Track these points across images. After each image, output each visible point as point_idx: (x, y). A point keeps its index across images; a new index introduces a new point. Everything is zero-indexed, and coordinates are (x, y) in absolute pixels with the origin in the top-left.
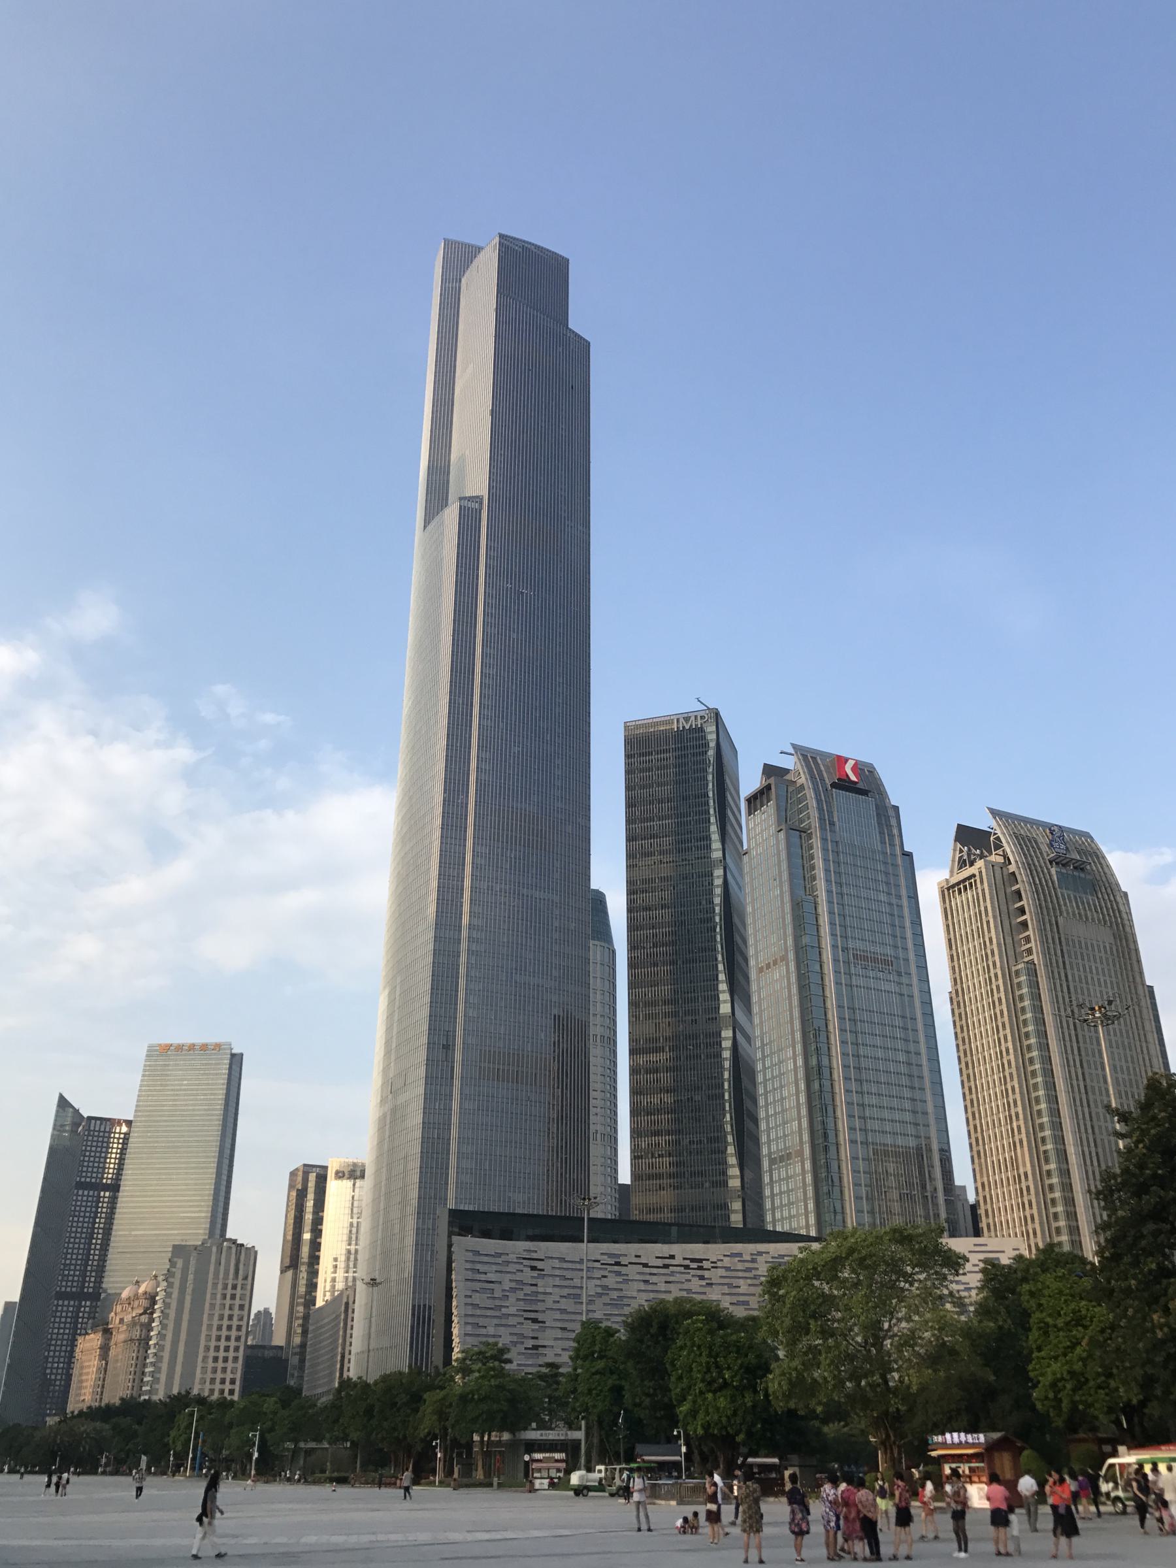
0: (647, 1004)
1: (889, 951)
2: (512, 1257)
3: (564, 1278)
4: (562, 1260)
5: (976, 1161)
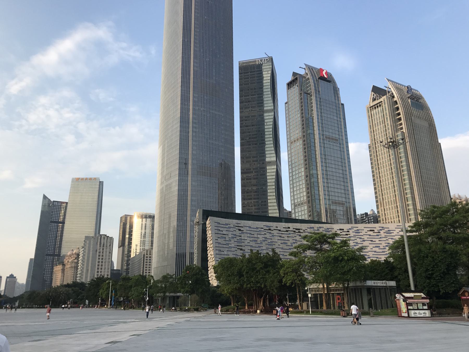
0: (247, 158)
1: (337, 136)
2: (232, 226)
4: (250, 227)
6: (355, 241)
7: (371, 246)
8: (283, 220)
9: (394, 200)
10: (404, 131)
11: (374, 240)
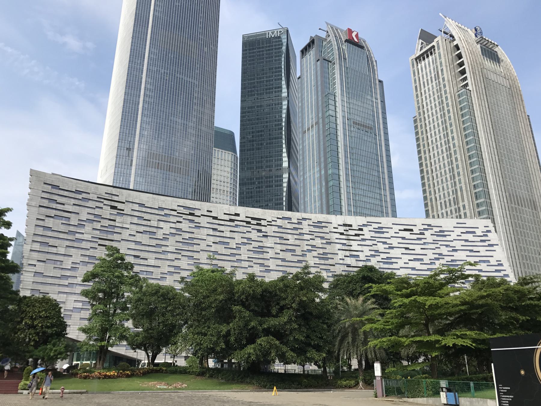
6: (375, 248)
7: (406, 258)
9: (454, 198)
10: (471, 89)
11: (411, 247)
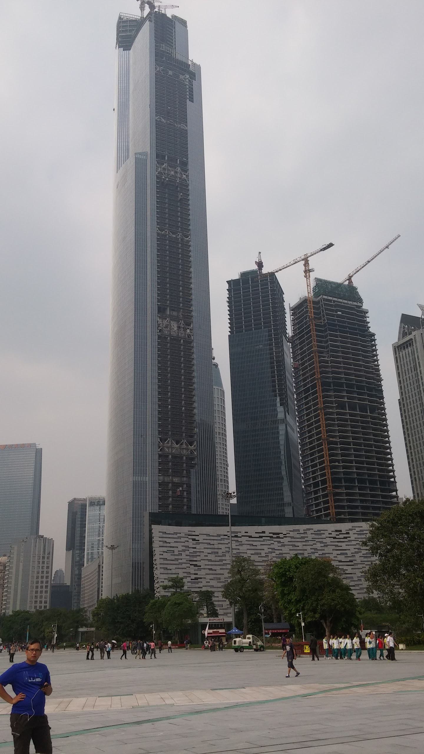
3: (210, 544)
5: (414, 483)
8: (263, 520)
